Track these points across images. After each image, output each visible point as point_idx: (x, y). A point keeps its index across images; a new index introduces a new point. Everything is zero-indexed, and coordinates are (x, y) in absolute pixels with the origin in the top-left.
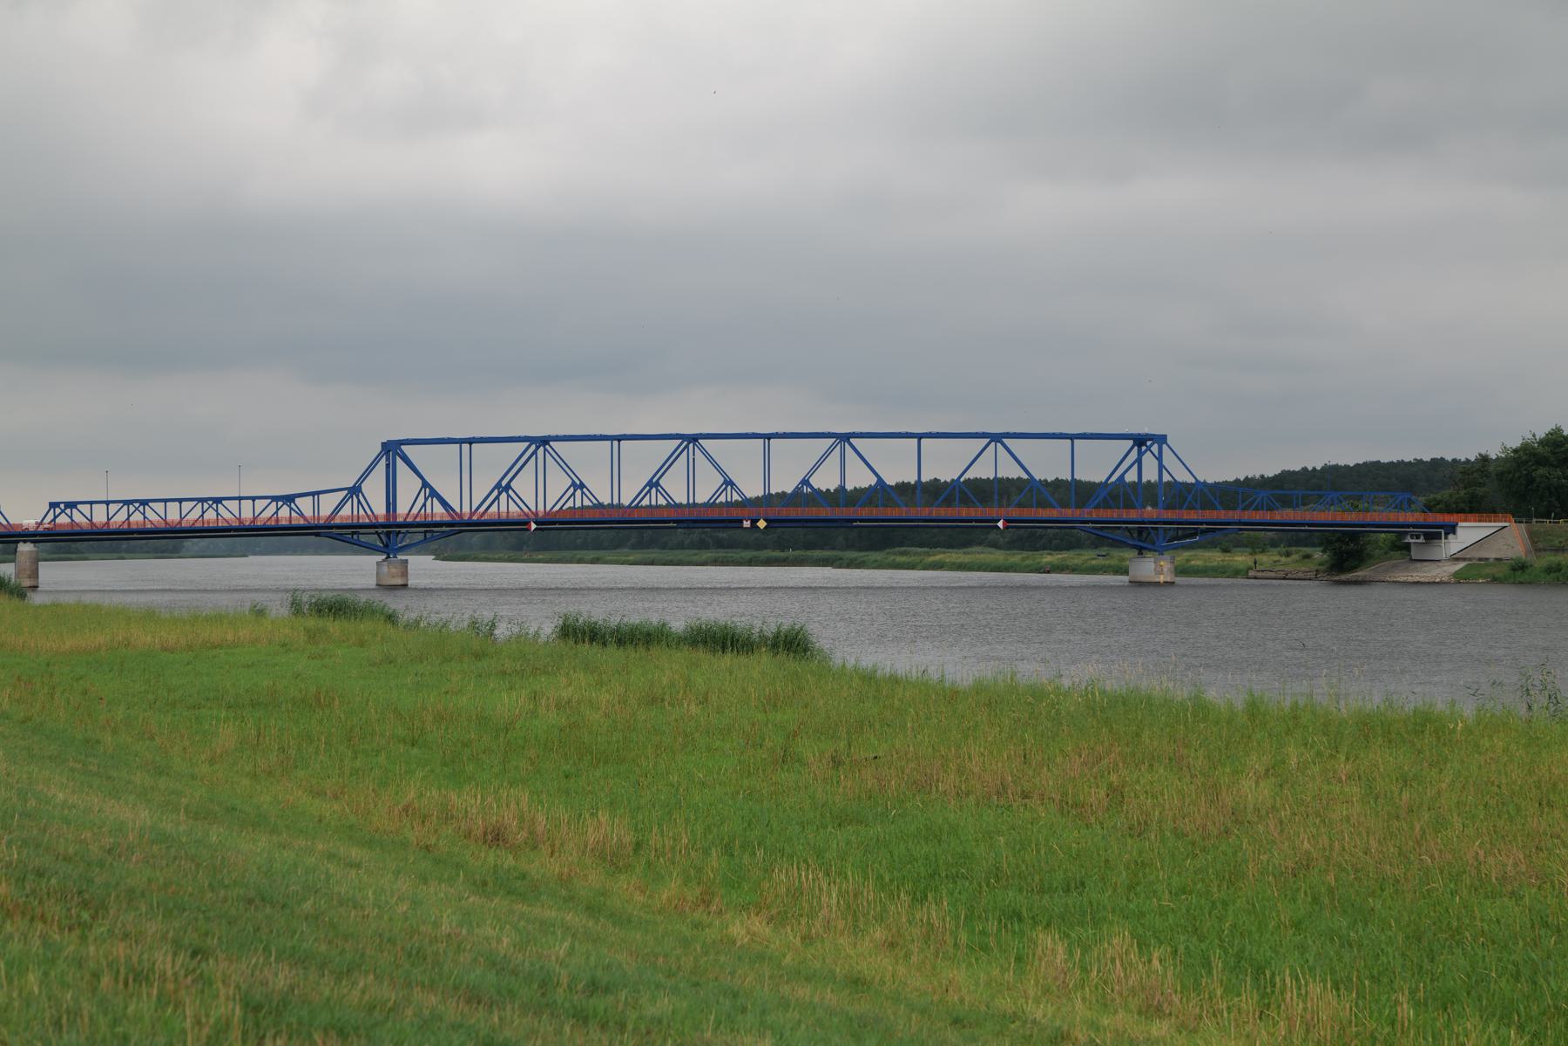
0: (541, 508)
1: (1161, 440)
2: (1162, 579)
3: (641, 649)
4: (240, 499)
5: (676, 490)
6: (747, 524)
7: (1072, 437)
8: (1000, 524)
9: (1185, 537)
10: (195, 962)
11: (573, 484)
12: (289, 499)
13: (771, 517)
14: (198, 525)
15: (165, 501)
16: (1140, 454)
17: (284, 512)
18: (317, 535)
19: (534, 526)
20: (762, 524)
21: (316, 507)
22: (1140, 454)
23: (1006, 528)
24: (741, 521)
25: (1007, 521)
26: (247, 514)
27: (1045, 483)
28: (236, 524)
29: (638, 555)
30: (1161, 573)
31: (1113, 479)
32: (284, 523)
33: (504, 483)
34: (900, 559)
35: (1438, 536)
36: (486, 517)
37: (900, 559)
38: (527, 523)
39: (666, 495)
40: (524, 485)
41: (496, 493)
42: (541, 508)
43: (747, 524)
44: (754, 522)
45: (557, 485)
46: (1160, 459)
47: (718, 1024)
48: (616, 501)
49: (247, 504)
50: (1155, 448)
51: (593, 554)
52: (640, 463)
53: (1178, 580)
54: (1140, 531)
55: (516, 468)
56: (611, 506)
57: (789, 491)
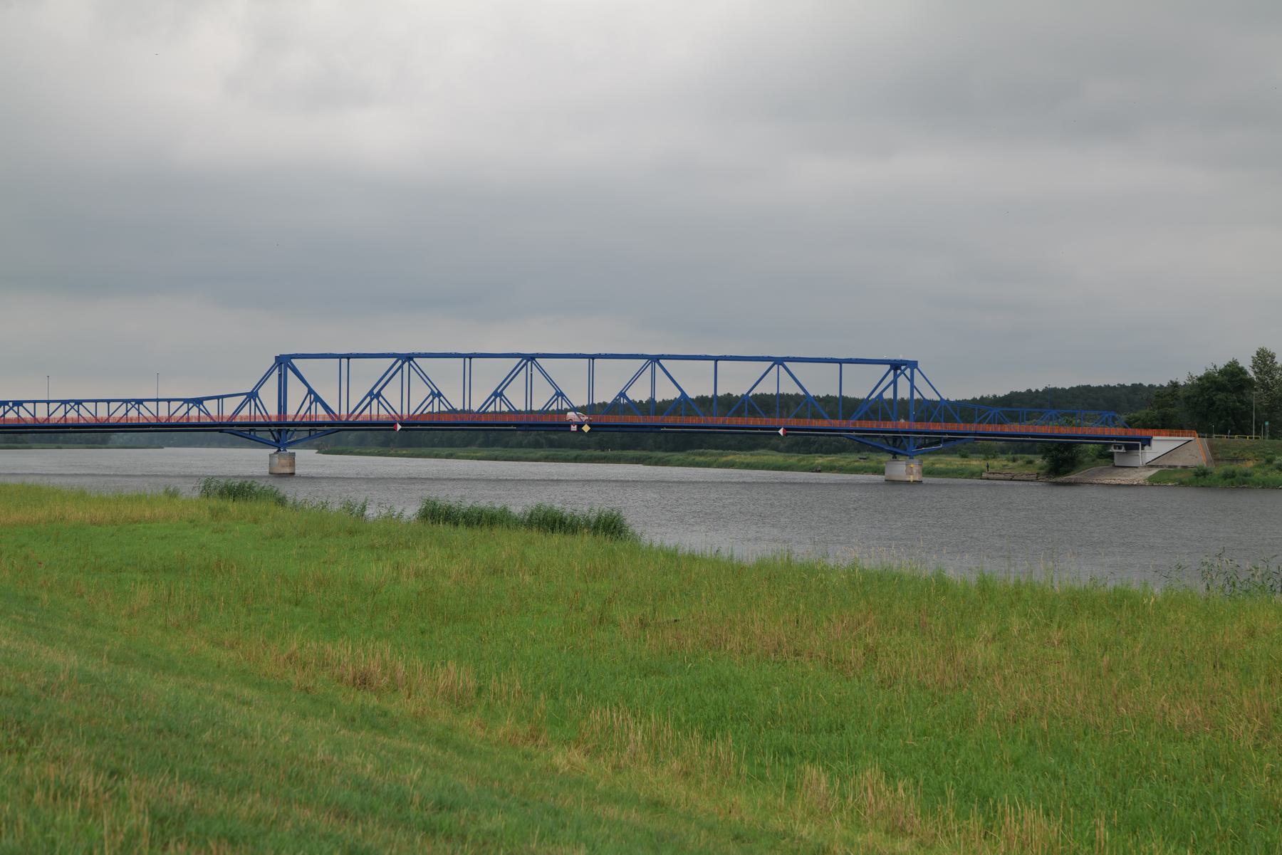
0: (405, 412)
1: (913, 365)
2: (911, 478)
4: (158, 400)
6: (574, 428)
7: (841, 362)
8: (781, 432)
9: (931, 445)
11: (432, 393)
12: (198, 402)
14: (123, 421)
16: (896, 376)
17: (194, 412)
19: (399, 427)
20: (586, 428)
21: (220, 408)
22: (896, 376)
23: (786, 435)
25: (786, 429)
26: (163, 413)
27: (817, 399)
28: (154, 421)
30: (911, 474)
31: (874, 396)
32: (194, 421)
34: (698, 459)
35: (1136, 447)
36: (360, 419)
37: (698, 459)
38: (394, 424)
40: (392, 393)
42: (405, 412)
43: (574, 428)
45: (419, 394)
46: (911, 380)
49: (163, 405)
50: (908, 372)
51: (447, 451)
52: (487, 377)
53: (927, 480)
54: (895, 439)
55: (385, 379)
56: (463, 411)
57: (609, 401)
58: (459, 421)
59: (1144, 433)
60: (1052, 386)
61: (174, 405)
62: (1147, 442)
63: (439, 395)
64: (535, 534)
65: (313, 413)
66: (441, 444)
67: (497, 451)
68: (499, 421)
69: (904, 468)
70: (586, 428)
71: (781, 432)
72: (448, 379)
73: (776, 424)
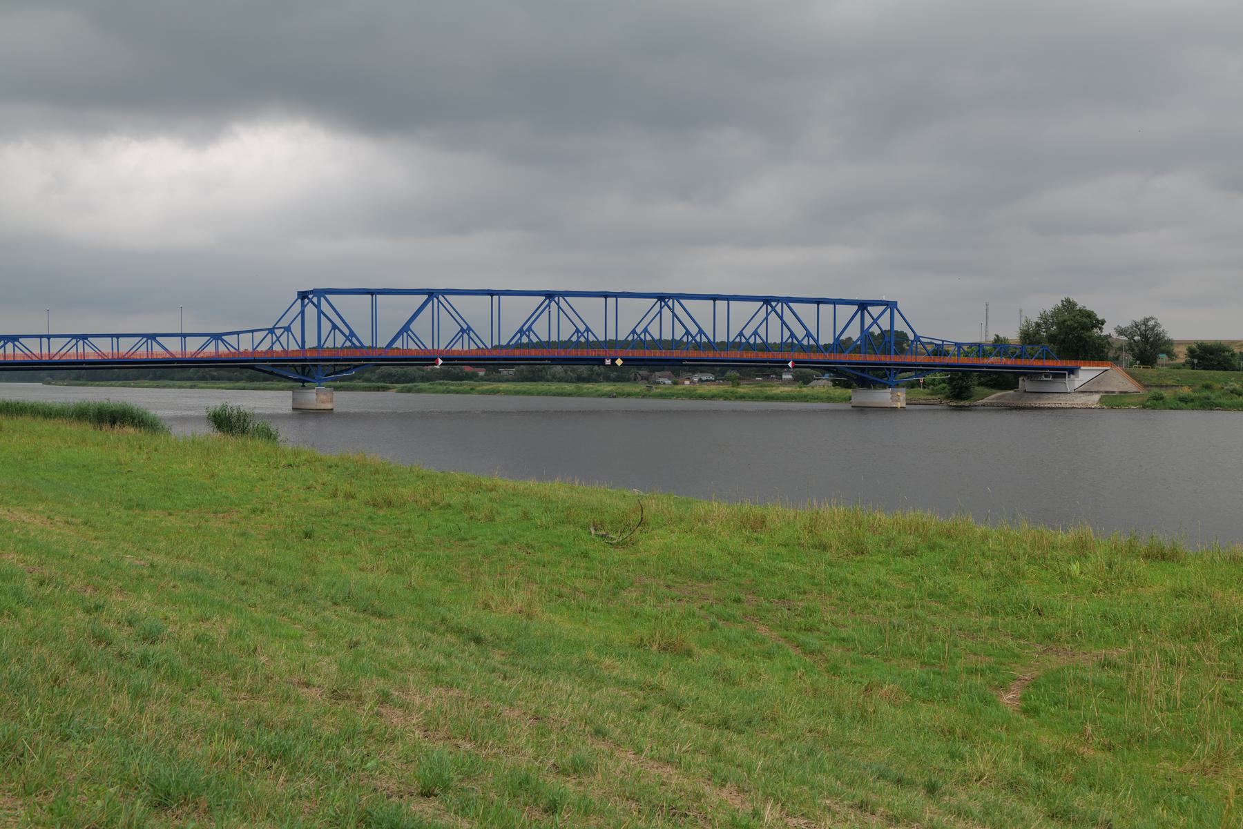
1: (895, 304)
2: (899, 405)
3: (108, 426)
5: (541, 331)
6: (608, 362)
8: (790, 364)
9: (342, 372)
11: (462, 330)
13: (625, 356)
15: (818, 302)
16: (303, 306)
19: (440, 362)
20: (619, 362)
21: (183, 345)
23: (794, 367)
24: (603, 360)
25: (795, 362)
29: (151, 383)
30: (898, 401)
35: (1063, 376)
36: (64, 358)
37: (440, 388)
38: (435, 359)
40: (421, 328)
43: (608, 362)
44: (614, 360)
45: (449, 329)
46: (318, 306)
47: (633, 770)
51: (189, 383)
52: (395, 311)
54: (304, 367)
55: (536, 314)
60: (1088, 308)
62: (1072, 371)
63: (469, 328)
64: (87, 428)
65: (80, 350)
66: (118, 379)
67: (166, 382)
71: (790, 364)
72: (475, 310)
73: (786, 357)
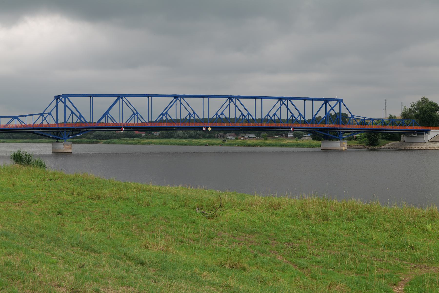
1: (342, 100)
2: (344, 149)
5: (172, 114)
6: (204, 129)
9: (76, 134)
10: (378, 283)
11: (134, 114)
12: (16, 118)
13: (212, 126)
16: (57, 103)
18: (32, 132)
20: (210, 129)
23: (294, 131)
24: (202, 128)
25: (294, 128)
30: (344, 146)
31: (159, 119)
33: (164, 113)
37: (123, 141)
38: (121, 128)
39: (112, 118)
40: (114, 112)
41: (78, 115)
43: (204, 129)
44: (207, 128)
45: (128, 113)
48: (150, 120)
50: (63, 100)
53: (349, 149)
54: (58, 132)
56: (90, 122)
58: (88, 127)
59: (426, 128)
61: (36, 117)
62: (427, 132)
63: (137, 113)
68: (80, 127)
69: (339, 144)
70: (210, 129)
71: (292, 129)
